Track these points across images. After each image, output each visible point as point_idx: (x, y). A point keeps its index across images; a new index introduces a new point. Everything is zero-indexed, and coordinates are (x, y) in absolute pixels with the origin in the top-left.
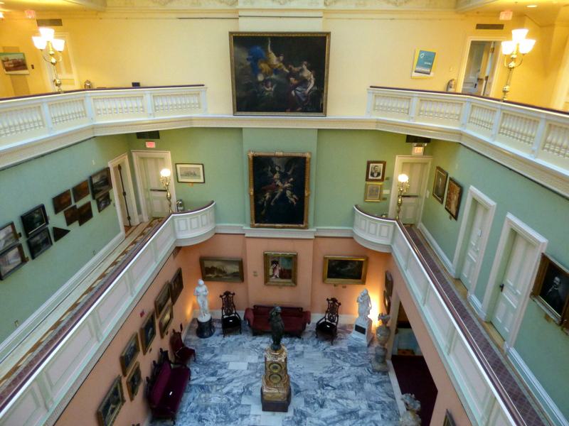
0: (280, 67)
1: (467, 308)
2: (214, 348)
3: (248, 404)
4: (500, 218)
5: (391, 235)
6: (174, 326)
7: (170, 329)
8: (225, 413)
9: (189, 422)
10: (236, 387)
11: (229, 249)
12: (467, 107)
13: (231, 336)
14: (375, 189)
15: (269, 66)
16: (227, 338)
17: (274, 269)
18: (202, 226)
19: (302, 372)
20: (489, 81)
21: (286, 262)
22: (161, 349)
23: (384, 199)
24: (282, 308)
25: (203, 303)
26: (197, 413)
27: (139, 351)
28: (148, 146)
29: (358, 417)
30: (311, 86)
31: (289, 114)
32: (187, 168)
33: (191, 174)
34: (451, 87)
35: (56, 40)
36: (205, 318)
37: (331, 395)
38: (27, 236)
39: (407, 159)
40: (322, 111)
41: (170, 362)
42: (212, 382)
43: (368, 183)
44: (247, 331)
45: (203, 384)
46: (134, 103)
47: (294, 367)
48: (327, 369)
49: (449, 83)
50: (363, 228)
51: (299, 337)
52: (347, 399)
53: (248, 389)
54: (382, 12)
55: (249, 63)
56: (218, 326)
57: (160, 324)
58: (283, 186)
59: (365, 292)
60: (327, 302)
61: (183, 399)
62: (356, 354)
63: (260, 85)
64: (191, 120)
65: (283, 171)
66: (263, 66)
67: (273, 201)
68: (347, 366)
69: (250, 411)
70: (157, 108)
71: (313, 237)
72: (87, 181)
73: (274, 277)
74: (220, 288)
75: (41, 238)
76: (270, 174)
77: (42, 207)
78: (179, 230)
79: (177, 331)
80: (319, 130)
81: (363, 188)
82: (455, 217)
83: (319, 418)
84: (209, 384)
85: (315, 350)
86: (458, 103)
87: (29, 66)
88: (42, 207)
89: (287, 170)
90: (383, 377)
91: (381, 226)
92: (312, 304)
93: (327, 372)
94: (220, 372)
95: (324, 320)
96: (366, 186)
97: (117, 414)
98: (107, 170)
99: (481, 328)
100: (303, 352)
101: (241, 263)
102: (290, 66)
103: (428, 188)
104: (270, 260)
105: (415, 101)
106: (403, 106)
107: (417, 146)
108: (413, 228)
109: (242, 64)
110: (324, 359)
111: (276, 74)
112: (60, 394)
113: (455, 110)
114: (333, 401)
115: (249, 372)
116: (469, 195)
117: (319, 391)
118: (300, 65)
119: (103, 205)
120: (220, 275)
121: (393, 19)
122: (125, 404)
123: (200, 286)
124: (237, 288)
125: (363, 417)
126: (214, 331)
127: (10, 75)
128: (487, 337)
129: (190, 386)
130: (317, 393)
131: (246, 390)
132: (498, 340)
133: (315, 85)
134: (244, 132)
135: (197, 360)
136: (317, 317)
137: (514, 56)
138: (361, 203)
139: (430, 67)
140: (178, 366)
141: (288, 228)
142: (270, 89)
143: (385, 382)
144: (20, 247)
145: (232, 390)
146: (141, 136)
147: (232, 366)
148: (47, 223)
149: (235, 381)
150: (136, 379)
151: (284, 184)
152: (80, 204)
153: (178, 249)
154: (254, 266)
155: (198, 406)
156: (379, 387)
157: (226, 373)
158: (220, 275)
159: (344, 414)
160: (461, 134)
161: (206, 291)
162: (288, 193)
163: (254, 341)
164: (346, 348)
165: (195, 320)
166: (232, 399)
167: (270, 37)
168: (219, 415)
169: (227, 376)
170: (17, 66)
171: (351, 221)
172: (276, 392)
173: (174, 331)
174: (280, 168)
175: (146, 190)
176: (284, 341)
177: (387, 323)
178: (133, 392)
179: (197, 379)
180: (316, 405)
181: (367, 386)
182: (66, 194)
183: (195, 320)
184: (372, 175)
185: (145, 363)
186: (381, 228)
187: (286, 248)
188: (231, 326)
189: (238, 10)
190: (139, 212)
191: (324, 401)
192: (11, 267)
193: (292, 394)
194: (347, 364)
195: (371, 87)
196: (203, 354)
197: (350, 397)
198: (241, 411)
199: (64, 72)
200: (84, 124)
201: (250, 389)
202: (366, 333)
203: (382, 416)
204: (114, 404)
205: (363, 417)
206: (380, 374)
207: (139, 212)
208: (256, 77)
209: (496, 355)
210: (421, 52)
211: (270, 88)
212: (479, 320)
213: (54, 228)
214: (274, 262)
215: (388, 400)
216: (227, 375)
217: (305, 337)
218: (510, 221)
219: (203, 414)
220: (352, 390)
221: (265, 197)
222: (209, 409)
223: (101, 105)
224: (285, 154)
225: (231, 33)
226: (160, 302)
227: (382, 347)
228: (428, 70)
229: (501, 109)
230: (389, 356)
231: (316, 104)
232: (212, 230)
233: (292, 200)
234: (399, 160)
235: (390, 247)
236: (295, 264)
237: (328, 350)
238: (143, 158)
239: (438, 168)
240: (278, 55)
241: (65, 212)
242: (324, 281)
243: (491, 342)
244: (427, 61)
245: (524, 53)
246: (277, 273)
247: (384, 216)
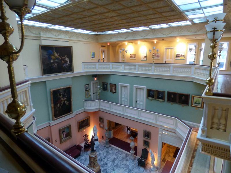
0: (58, 57)
5: (98, 105)
15: (55, 57)
23: (90, 96)
29: (116, 159)
30: (68, 63)
31: (62, 73)
37: (105, 160)
40: (72, 71)
52: (110, 158)
54: (82, 41)
55: (47, 56)
62: (99, 148)
63: (52, 64)
65: (63, 94)
66: (53, 57)
67: (61, 106)
70: (195, 73)
73: (63, 139)
76: (59, 96)
83: (109, 167)
114: (108, 161)
117: (102, 162)
125: (117, 158)
133: (69, 63)
134: (47, 83)
139: (94, 56)
142: (55, 65)
151: (64, 99)
159: (113, 161)
162: (66, 102)
174: (62, 93)
180: (105, 165)
181: (110, 152)
184: (86, 89)
186: (92, 104)
187: (66, 124)
191: (106, 163)
197: (110, 157)
203: (120, 154)
205: (117, 158)
208: (50, 61)
210: (92, 52)
211: (55, 65)
215: (117, 151)
228: (94, 57)
231: (70, 69)
233: (67, 104)
240: (57, 53)
246: (64, 136)
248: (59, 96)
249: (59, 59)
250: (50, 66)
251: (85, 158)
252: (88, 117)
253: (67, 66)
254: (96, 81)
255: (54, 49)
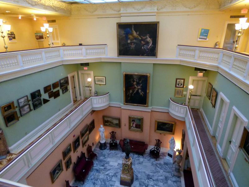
0: (137, 37)
1: (214, 150)
2: (105, 155)
3: (115, 180)
4: (230, 109)
6: (89, 143)
7: (87, 144)
8: (104, 183)
9: (90, 184)
10: (111, 173)
11: (114, 113)
12: (221, 54)
13: (113, 151)
14: (179, 91)
15: (133, 36)
16: (111, 151)
17: (133, 124)
18: (103, 102)
19: (140, 171)
20: (238, 42)
21: (138, 121)
22: (82, 152)
24: (130, 140)
25: (102, 135)
26: (93, 181)
27: (71, 151)
28: (84, 69)
30: (151, 44)
31: (141, 57)
32: (99, 78)
33: (101, 80)
34: (217, 45)
35: (49, 28)
36: (103, 142)
38: (33, 101)
39: (195, 78)
41: (86, 158)
42: (102, 169)
43: (176, 88)
44: (120, 149)
45: (98, 169)
46: (79, 52)
47: (137, 168)
48: (152, 171)
49: (216, 43)
50: (173, 109)
51: (142, 155)
53: (116, 174)
56: (108, 145)
57: (82, 141)
58: (138, 88)
59: (173, 138)
60: (156, 141)
61: (89, 174)
62: (167, 166)
64: (101, 59)
65: (138, 81)
66: (130, 36)
68: (161, 171)
69: (115, 184)
70: (180, 55)
71: (150, 111)
72: (58, 81)
73: (133, 127)
74: (110, 129)
75: (38, 102)
76: (132, 82)
77: (39, 91)
78: (94, 104)
79: (90, 145)
80: (154, 64)
81: (174, 90)
82: (214, 106)
84: (100, 170)
85: (148, 162)
86: (217, 53)
87: (44, 38)
88: (39, 91)
89: (139, 81)
90: (178, 179)
91: (181, 108)
92: (150, 141)
93: (152, 172)
94: (106, 165)
95: (154, 149)
96: (176, 90)
97: (59, 174)
98: (67, 78)
99: (219, 161)
100: (143, 162)
101: (119, 120)
102: (141, 36)
103: (205, 93)
104: (131, 120)
105: (197, 52)
106: (192, 54)
107: (200, 72)
108: (198, 110)
109: (121, 36)
110: (152, 166)
111: (136, 40)
112: (35, 162)
113: (216, 56)
114: (152, 186)
115: (117, 167)
116: (220, 96)
117: (147, 180)
118: (146, 35)
119: (65, 91)
120: (111, 124)
121: (188, 15)
122: (63, 171)
123: (101, 128)
124: (117, 130)
126: (107, 147)
127: (38, 41)
128: (221, 166)
129: (93, 169)
130: (145, 181)
131: (115, 174)
132: (226, 167)
133: (152, 44)
134: (122, 63)
135: (97, 159)
136: (151, 147)
137: (240, 31)
138: (173, 97)
139: (207, 36)
140: (89, 160)
141: (139, 106)
142: (133, 46)
143: (178, 181)
144: (29, 105)
145: (109, 174)
146: (82, 64)
147: (111, 163)
148: (41, 97)
149: (111, 170)
150: (69, 162)
151: (138, 87)
152: (55, 90)
153: (93, 112)
154: (125, 122)
155: (94, 178)
156: (175, 183)
157: (108, 166)
158: (111, 124)
160: (218, 67)
161: (103, 130)
162: (140, 91)
163: (122, 154)
164: (163, 163)
165: (99, 142)
166: (108, 178)
167: (134, 24)
168: (102, 183)
169: (108, 167)
170: (41, 38)
171: (168, 105)
172: (127, 178)
173: (89, 145)
174: (136, 79)
175: (83, 87)
176: (131, 155)
177: (180, 153)
178: (67, 167)
179: (96, 166)
181: (169, 182)
182: (49, 86)
183: (99, 142)
185: (74, 156)
188: (113, 146)
189: (120, 13)
190: (80, 95)
192: (25, 112)
193: (135, 179)
194: (162, 171)
195: (178, 45)
196: (100, 156)
198: (111, 183)
199: (56, 39)
200: (59, 59)
201: (117, 174)
202: (173, 157)
204: (58, 171)
206: (177, 177)
207: (80, 95)
208: (127, 41)
209: (223, 175)
210: (202, 29)
211: (133, 46)
212: (220, 157)
213: (43, 99)
214: (133, 121)
216: (109, 167)
217: (145, 156)
218: (234, 110)
219: (96, 182)
220: (162, 182)
221: (130, 92)
222: (98, 180)
223: (66, 52)
224: (139, 74)
225: (117, 23)
226: (83, 132)
227: (178, 165)
228: (206, 38)
229: (234, 56)
230: (182, 169)
231: (152, 52)
232: (107, 105)
233: (141, 94)
234: (191, 79)
235: (184, 118)
236: (142, 122)
237: (154, 163)
238: (82, 74)
239: (210, 83)
240: (136, 32)
241: (48, 93)
242: (155, 131)
243: (222, 168)
244: (205, 34)
245: (244, 29)
246: (134, 125)
247: (183, 104)
248: (132, 82)
249: (138, 38)
250: (127, 46)
251: (143, 161)
252: (174, 122)
253: (148, 49)
254: (200, 77)
255: (133, 26)
